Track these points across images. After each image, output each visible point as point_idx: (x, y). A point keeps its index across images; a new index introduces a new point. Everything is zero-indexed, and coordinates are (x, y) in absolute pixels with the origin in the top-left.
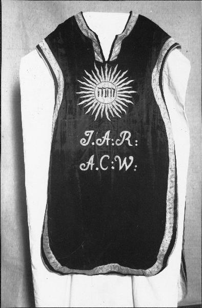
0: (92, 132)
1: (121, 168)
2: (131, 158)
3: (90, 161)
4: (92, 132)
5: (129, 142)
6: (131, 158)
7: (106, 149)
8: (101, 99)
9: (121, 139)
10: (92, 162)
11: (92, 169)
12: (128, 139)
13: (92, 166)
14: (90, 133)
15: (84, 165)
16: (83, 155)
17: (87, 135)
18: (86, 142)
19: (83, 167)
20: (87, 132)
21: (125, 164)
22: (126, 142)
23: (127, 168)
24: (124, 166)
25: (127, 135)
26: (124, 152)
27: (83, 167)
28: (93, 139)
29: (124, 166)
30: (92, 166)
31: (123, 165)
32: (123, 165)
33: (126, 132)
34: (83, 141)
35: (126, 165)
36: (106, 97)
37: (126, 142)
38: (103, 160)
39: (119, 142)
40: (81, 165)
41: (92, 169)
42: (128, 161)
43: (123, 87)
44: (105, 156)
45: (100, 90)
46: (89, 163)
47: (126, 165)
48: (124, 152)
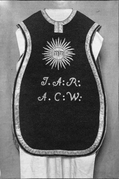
0: (47, 78)
1: (72, 99)
2: (78, 94)
3: (59, 80)
4: (47, 78)
5: (76, 84)
6: (78, 94)
7: (58, 88)
8: (55, 57)
9: (70, 82)
10: (60, 81)
11: (60, 85)
12: (75, 82)
13: (60, 84)
14: (46, 79)
15: (55, 82)
16: (41, 90)
17: (45, 79)
18: (45, 83)
19: (54, 84)
20: (44, 78)
21: (74, 97)
22: (73, 84)
23: (76, 99)
24: (74, 98)
25: (74, 80)
26: (73, 89)
27: (54, 84)
28: (48, 81)
29: (74, 98)
30: (60, 84)
31: (73, 98)
32: (73, 98)
33: (73, 78)
34: (43, 83)
35: (75, 98)
36: (58, 56)
37: (73, 84)
38: (57, 96)
39: (68, 84)
40: (39, 97)
41: (60, 85)
42: (76, 96)
43: (50, 49)
44: (57, 93)
45: (55, 53)
46: (58, 82)
47: (75, 98)
48: (73, 89)
